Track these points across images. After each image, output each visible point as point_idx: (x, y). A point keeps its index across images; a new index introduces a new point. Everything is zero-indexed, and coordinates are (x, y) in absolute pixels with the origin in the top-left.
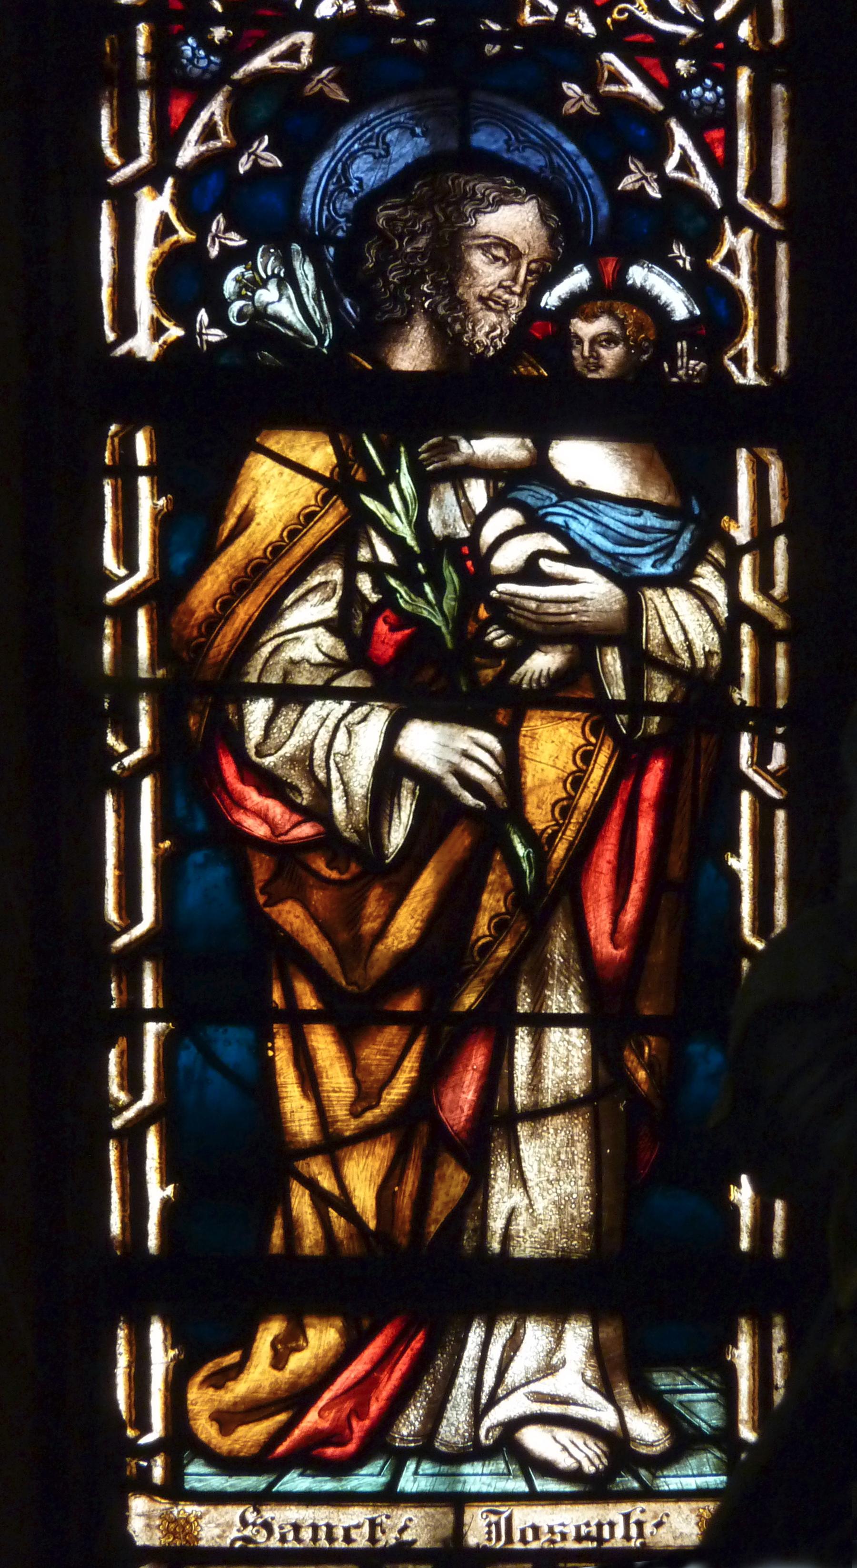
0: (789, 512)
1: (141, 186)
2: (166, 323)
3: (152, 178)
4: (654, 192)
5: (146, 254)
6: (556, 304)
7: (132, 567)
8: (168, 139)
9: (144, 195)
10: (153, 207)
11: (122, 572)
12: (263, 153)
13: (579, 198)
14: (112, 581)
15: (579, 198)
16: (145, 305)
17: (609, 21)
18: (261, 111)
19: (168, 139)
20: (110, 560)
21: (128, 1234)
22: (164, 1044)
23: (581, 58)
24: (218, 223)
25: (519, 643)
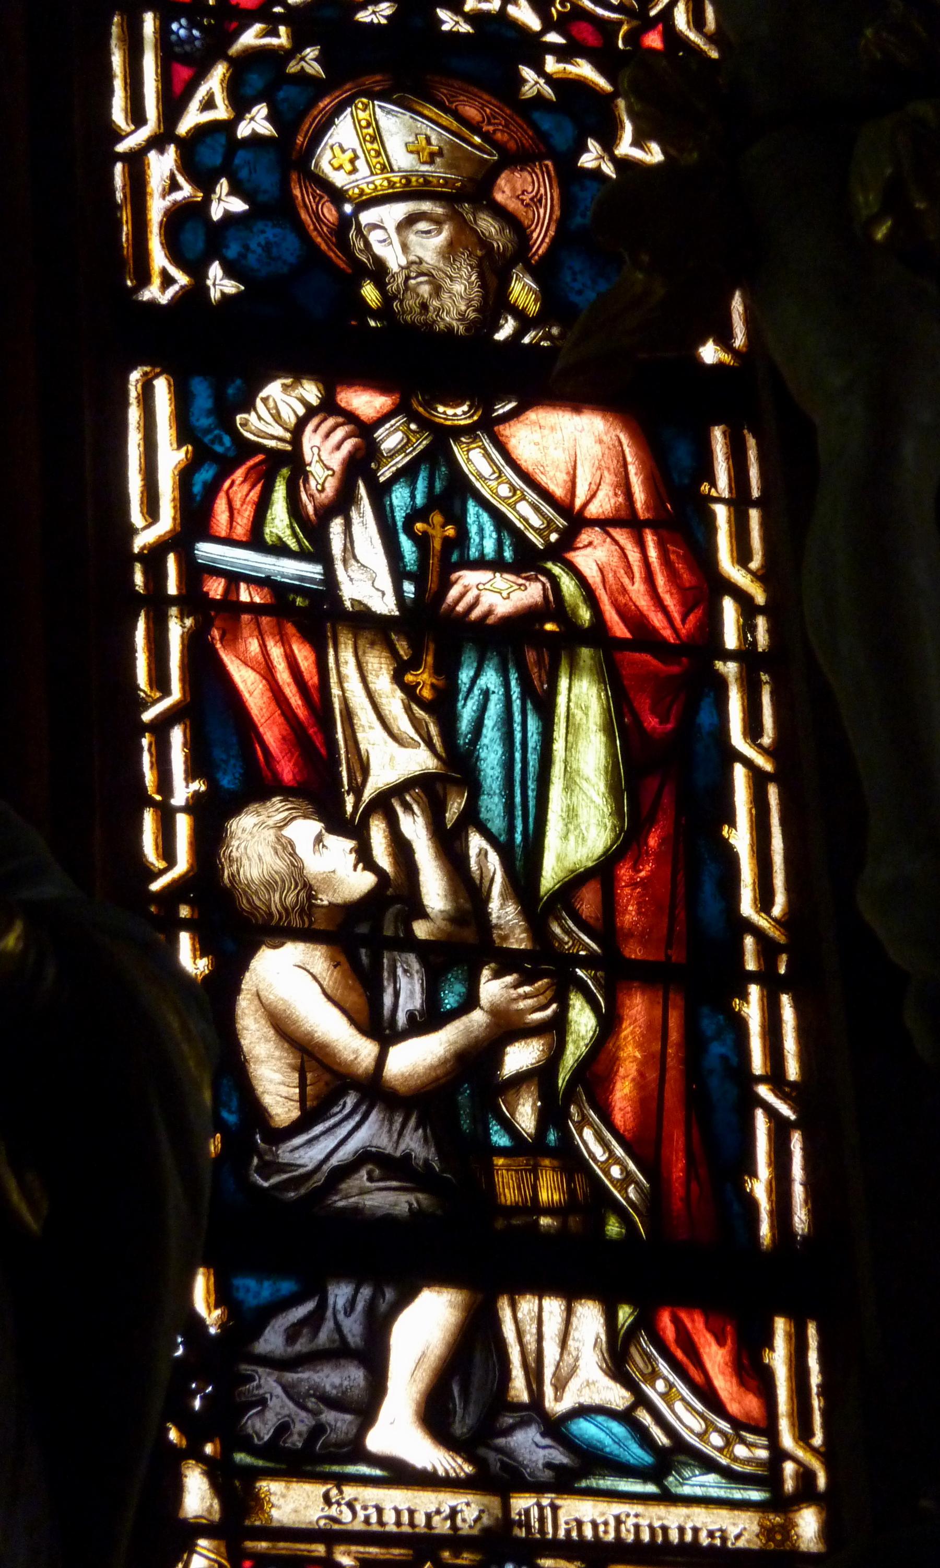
0: (764, 488)
1: (149, 151)
2: (181, 179)
3: (157, 143)
4: (608, 169)
5: (157, 208)
6: (443, 908)
7: (166, 691)
8: (173, 107)
9: (152, 155)
10: (160, 165)
11: (161, 865)
12: (257, 122)
13: (538, 230)
14: (145, 705)
15: (538, 230)
16: (159, 258)
17: (553, 10)
18: (256, 81)
19: (173, 107)
20: (137, 518)
21: (188, 695)
22: (227, 88)
23: (531, 49)
24: (223, 186)
25: (537, 627)
